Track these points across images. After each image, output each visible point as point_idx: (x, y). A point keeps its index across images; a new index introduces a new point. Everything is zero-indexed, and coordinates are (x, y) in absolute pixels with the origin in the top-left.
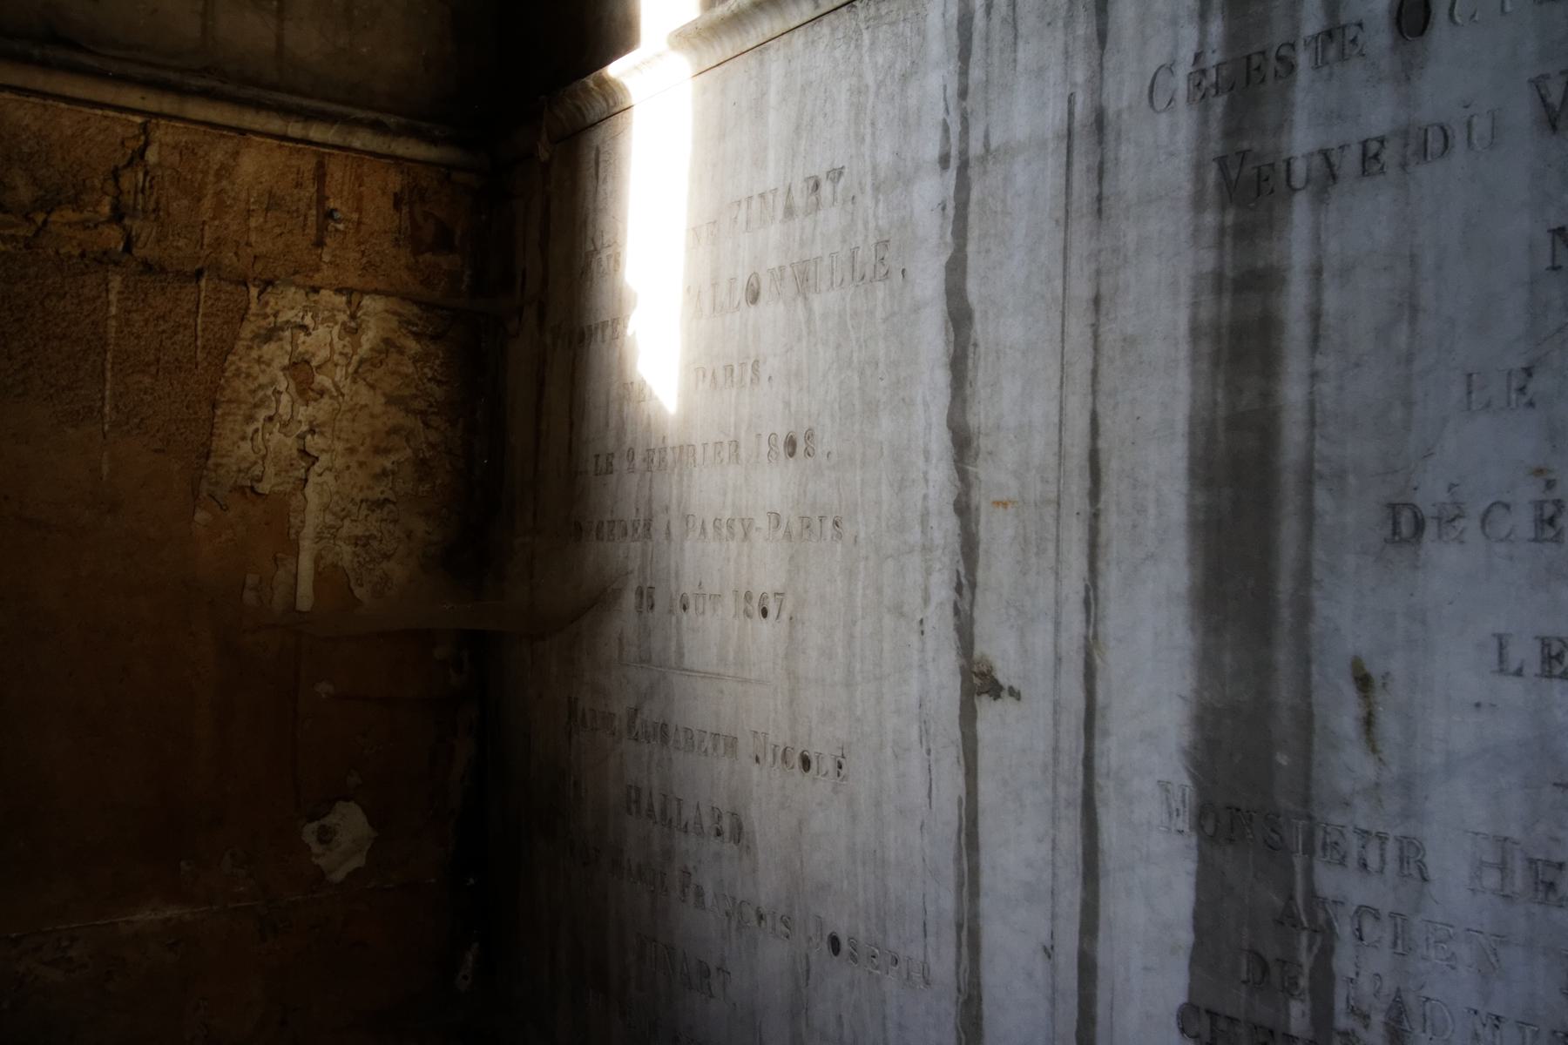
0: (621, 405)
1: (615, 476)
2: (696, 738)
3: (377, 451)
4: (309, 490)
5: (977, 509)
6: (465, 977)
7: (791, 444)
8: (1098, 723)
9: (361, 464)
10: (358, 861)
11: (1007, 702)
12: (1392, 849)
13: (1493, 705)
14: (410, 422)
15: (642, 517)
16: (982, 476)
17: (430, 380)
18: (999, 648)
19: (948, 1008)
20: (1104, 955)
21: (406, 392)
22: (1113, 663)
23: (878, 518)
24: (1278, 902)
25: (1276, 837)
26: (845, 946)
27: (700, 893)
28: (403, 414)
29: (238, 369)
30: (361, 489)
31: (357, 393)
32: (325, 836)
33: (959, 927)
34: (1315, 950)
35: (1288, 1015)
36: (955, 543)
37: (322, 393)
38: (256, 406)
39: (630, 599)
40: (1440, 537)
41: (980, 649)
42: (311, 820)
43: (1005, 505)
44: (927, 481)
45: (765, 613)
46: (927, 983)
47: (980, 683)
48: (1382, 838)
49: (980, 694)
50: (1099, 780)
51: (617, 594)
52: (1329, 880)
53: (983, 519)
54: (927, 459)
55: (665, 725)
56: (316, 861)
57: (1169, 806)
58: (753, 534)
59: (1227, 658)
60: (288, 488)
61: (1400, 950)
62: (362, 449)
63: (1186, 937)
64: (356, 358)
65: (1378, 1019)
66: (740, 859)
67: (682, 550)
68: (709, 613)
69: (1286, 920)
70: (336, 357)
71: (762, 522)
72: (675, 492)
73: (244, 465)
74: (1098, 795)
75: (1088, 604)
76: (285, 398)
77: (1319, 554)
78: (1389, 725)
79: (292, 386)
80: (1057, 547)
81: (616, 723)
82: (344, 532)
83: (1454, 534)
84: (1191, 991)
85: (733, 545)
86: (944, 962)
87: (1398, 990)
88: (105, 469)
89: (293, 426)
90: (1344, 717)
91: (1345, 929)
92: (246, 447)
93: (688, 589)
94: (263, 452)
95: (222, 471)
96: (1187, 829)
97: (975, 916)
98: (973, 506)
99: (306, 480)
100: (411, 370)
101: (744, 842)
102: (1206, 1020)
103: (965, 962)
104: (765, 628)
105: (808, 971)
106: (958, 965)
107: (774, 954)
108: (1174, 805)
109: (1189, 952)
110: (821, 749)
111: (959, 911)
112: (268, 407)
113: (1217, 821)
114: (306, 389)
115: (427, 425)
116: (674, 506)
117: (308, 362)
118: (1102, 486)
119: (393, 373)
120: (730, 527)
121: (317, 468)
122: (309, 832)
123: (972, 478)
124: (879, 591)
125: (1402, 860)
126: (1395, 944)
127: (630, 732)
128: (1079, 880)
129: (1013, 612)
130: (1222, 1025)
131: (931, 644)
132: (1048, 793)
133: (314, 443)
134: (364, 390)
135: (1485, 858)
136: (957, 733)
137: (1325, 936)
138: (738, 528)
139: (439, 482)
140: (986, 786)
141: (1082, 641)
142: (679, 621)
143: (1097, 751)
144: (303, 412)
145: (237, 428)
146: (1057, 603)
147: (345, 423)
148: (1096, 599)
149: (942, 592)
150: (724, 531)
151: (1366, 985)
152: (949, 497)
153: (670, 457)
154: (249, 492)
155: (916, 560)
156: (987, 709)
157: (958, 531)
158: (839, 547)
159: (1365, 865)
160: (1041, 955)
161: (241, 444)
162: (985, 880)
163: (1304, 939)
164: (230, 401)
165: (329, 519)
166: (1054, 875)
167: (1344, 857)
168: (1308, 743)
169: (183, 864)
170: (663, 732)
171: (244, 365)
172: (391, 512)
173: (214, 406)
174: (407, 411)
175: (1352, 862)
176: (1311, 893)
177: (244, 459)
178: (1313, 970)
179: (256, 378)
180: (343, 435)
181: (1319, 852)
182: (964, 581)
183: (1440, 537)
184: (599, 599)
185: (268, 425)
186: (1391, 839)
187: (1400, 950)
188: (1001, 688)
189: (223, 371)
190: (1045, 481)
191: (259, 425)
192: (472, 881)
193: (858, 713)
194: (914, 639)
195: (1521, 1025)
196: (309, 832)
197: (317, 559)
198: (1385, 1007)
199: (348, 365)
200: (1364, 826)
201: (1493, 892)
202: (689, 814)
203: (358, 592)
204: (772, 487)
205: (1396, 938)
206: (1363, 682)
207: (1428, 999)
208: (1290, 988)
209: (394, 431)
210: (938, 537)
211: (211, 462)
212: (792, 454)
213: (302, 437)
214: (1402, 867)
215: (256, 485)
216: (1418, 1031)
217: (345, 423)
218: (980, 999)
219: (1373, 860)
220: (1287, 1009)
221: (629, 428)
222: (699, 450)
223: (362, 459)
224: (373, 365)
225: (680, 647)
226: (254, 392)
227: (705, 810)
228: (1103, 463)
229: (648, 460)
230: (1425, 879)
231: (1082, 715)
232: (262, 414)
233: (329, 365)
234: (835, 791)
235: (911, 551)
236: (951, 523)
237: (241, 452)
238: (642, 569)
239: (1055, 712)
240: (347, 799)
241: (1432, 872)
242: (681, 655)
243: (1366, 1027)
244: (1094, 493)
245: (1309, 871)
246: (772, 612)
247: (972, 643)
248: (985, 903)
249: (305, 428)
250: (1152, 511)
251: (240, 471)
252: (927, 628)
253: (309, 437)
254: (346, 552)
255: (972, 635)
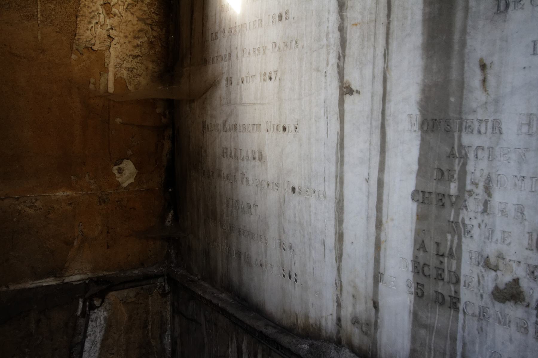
0: (220, 14)
1: (217, 41)
2: (246, 128)
3: (135, 37)
4: (111, 50)
5: (346, 28)
6: (169, 222)
7: (281, 16)
8: (387, 98)
9: (129, 42)
10: (132, 180)
11: (355, 95)
12: (490, 124)
13: (530, 67)
14: (148, 28)
15: (228, 53)
16: (349, 15)
17: (153, 13)
18: (353, 77)
19: (332, 205)
20: (386, 178)
21: (145, 17)
22: (393, 75)
23: (311, 37)
24: (448, 150)
25: (449, 127)
26: (297, 190)
27: (248, 180)
28: (144, 25)
29: (85, 4)
30: (130, 51)
31: (127, 16)
32: (120, 171)
33: (337, 177)
34: (461, 164)
35: (450, 188)
36: (338, 42)
37: (115, 15)
38: (91, 18)
39: (224, 82)
40: (515, 8)
41: (346, 78)
42: (115, 165)
43: (356, 25)
44: (328, 21)
45: (271, 79)
46: (325, 198)
47: (346, 90)
48: (486, 121)
49: (346, 94)
50: (387, 118)
51: (219, 81)
52: (467, 139)
53: (348, 31)
54: (329, 13)
55: (236, 124)
56: (118, 179)
57: (411, 122)
58: (267, 51)
59: (434, 67)
60: (104, 48)
61: (490, 159)
62: (129, 36)
63: (415, 167)
64: (126, 3)
65: (481, 185)
66: (262, 166)
67: (242, 61)
68: (251, 82)
69: (451, 156)
70: (119, 2)
71: (270, 46)
72: (239, 41)
73: (88, 39)
74: (386, 123)
75: (385, 55)
76: (102, 16)
77: (470, 23)
78: (492, 81)
79: (104, 11)
80: (375, 37)
81: (219, 127)
82: (124, 66)
83: (520, 6)
84: (417, 185)
85: (260, 56)
86: (331, 191)
87: (489, 173)
88: (39, 37)
89: (105, 26)
90: (474, 78)
91: (471, 155)
92: (89, 32)
93: (244, 75)
94: (95, 35)
95: (81, 41)
96: (417, 130)
97: (342, 172)
98: (345, 27)
99: (110, 46)
100: (146, 9)
101: (263, 160)
102: (421, 194)
103: (338, 188)
104: (271, 84)
105: (284, 200)
106: (336, 190)
107: (273, 196)
108: (413, 123)
109: (416, 172)
110: (290, 123)
111: (337, 171)
112: (96, 19)
113: (428, 125)
114: (109, 13)
115: (152, 29)
116: (239, 47)
117: (109, 3)
118: (392, 12)
119: (140, 9)
120: (259, 50)
121: (114, 42)
122: (115, 169)
123: (345, 17)
124: (311, 64)
125: (493, 128)
126: (489, 158)
127: (224, 129)
128: (379, 153)
129: (358, 63)
130: (427, 195)
131: (329, 79)
132: (369, 126)
133: (113, 33)
134: (130, 15)
135: (523, 122)
136: (337, 110)
137: (464, 158)
138: (261, 50)
139: (157, 50)
140: (347, 126)
141: (383, 69)
142: (241, 88)
143: (386, 108)
144: (108, 22)
145: (85, 26)
146: (374, 57)
147: (123, 27)
148: (388, 53)
149: (333, 60)
150: (257, 52)
151: (478, 173)
152: (336, 26)
153: (237, 30)
154: (90, 49)
155: (324, 50)
156: (348, 99)
157: (339, 37)
158: (297, 50)
159: (480, 132)
160: (365, 182)
161: (87, 31)
162: (346, 159)
163: (457, 161)
164: (82, 16)
165: (119, 61)
166: (370, 154)
167: (472, 130)
168: (462, 92)
169: (72, 177)
170: (235, 127)
171: (87, 3)
172: (140, 60)
173: (77, 17)
174: (146, 24)
175: (475, 132)
176: (461, 146)
177: (88, 37)
178: (459, 171)
179: (91, 8)
180: (123, 31)
181: (464, 130)
182: (341, 55)
183: (515, 8)
184: (212, 85)
185: (96, 25)
186: (490, 121)
187: (490, 159)
188: (353, 91)
189: (80, 5)
190: (371, 13)
191: (93, 25)
192: (170, 190)
193: (303, 108)
194: (323, 79)
195: (532, 178)
196: (115, 169)
197: (115, 75)
198: (484, 180)
199: (124, 5)
200: (480, 118)
201: (525, 134)
202: (244, 154)
203: (129, 87)
204: (275, 33)
205: (489, 155)
206: (483, 67)
207: (499, 175)
208: (451, 179)
209: (140, 31)
210: (332, 41)
211: (76, 38)
212: (281, 20)
213: (108, 30)
214: (493, 131)
215: (93, 47)
216: (495, 186)
217: (123, 27)
218: (343, 200)
219: (483, 130)
220: (450, 186)
221: (223, 22)
222: (248, 25)
223: (130, 40)
224: (133, 6)
225: (241, 96)
226: (90, 13)
227: (250, 151)
228: (392, 4)
229: (230, 32)
230: (501, 133)
231: (382, 96)
232: (94, 21)
233: (117, 5)
234: (294, 137)
235: (322, 48)
236: (337, 34)
237: (86, 35)
238: (228, 71)
239: (372, 96)
240: (127, 159)
241: (504, 130)
242: (241, 99)
243: (477, 188)
244: (389, 16)
245: (460, 137)
246: (273, 78)
247: (343, 77)
248: (346, 167)
249: (109, 27)
250: (409, 18)
251: (87, 41)
252: (327, 74)
253: (111, 31)
254: (125, 74)
255: (343, 74)
